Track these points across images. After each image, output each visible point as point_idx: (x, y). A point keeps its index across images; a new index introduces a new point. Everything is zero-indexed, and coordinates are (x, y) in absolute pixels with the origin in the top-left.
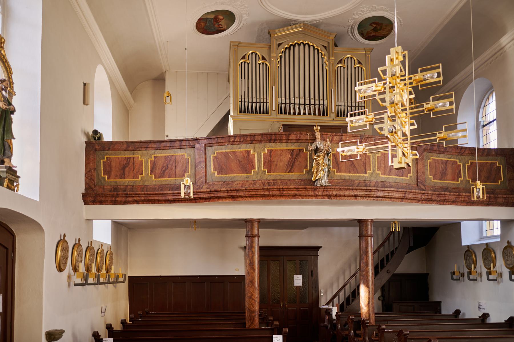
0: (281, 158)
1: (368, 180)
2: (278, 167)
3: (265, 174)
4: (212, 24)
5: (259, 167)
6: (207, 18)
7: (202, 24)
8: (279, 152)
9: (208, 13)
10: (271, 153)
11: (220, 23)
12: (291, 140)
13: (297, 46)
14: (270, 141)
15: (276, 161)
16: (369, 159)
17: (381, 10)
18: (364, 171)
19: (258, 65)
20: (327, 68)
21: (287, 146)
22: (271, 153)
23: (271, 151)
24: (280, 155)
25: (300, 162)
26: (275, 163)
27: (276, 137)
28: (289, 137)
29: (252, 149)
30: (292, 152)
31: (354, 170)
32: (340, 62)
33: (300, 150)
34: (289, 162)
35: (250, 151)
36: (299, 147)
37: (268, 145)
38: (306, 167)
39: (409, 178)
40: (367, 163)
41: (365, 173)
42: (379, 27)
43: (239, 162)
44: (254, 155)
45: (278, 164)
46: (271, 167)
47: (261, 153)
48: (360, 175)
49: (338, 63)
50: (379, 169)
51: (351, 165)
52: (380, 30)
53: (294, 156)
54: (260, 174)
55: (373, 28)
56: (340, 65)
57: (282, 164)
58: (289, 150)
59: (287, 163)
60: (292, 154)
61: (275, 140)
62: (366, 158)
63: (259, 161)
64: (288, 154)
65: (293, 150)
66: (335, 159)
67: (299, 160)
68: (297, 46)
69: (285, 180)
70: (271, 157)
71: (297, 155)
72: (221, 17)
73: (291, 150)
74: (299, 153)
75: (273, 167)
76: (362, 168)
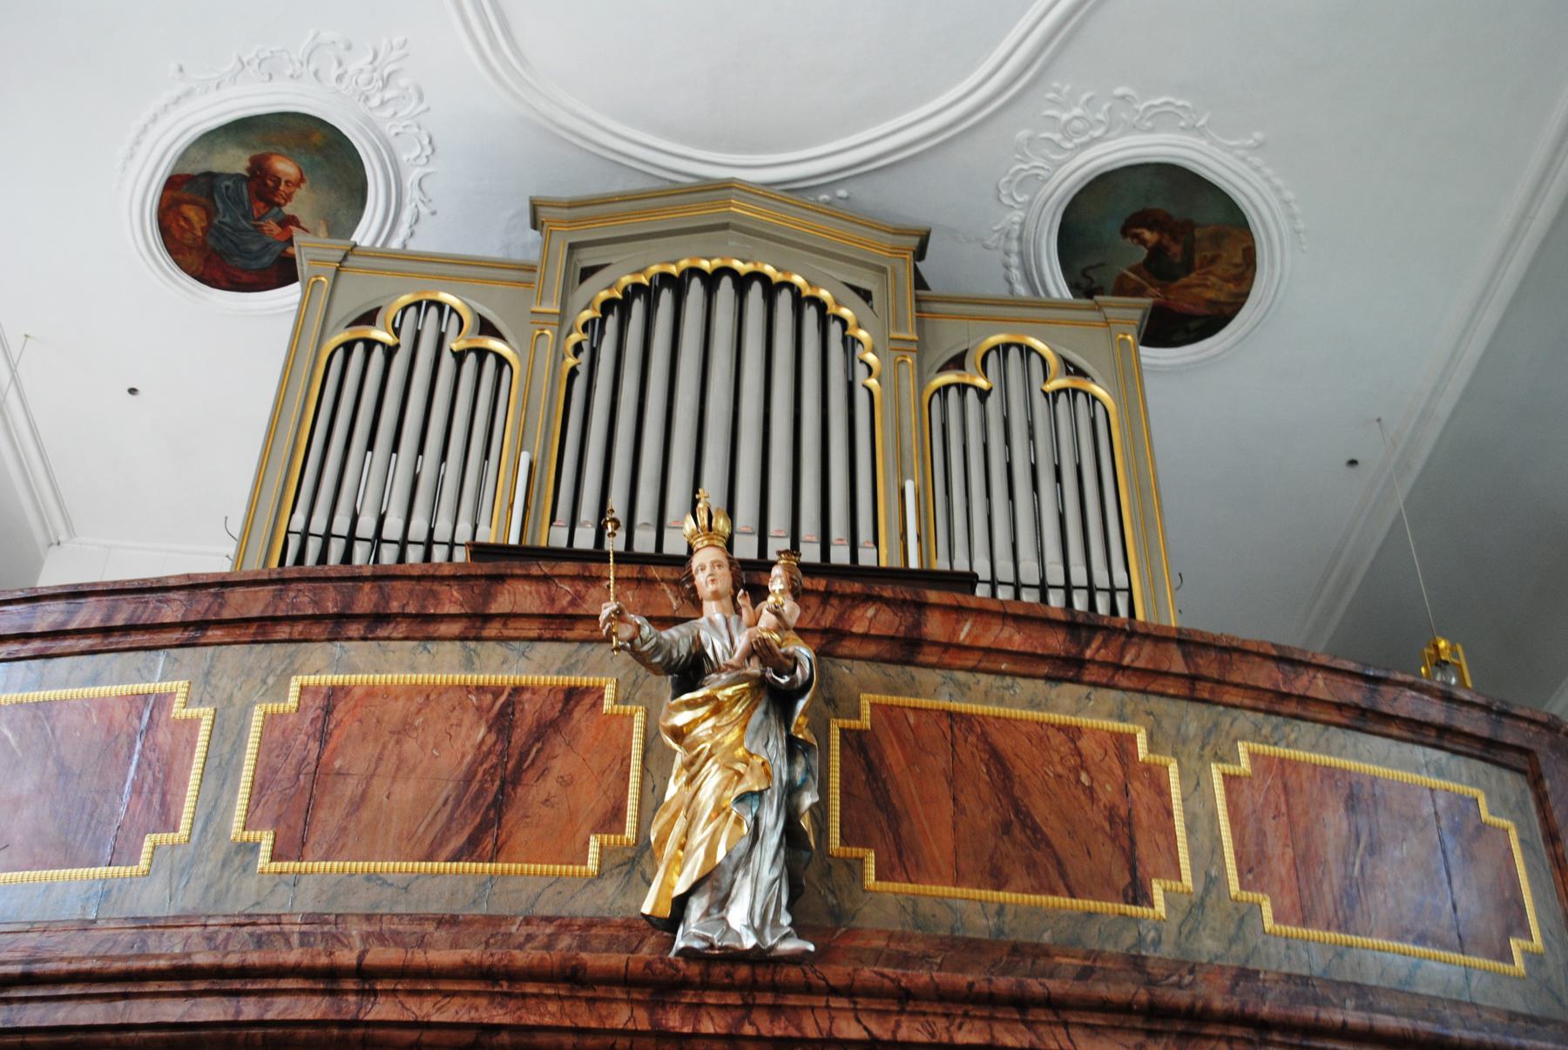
0: (410, 746)
1: (1167, 950)
2: (366, 814)
3: (246, 868)
4: (242, 208)
5: (212, 814)
6: (210, 176)
7: (192, 212)
8: (398, 707)
9: (212, 139)
10: (328, 710)
11: (288, 209)
12: (506, 617)
13: (696, 288)
14: (336, 625)
15: (360, 767)
16: (1163, 792)
17: (1162, 118)
18: (1122, 879)
19: (447, 362)
20: (873, 382)
21: (469, 665)
22: (328, 710)
23: (334, 694)
24: (404, 729)
25: (566, 782)
26: (350, 788)
27: (386, 599)
28: (488, 597)
29: (166, 677)
30: (503, 709)
31: (1031, 866)
32: (958, 362)
33: (572, 695)
34: (468, 778)
35: (162, 701)
36: (568, 669)
37: (318, 653)
38: (613, 819)
39: (1519, 964)
40: (1142, 815)
41: (1139, 894)
42: (1176, 249)
43: (63, 771)
44: (194, 724)
45: (379, 790)
46: (310, 809)
47: (246, 713)
48: (1091, 905)
49: (944, 369)
50: (1251, 869)
51: (1006, 828)
52: (1188, 267)
53: (519, 736)
54: (208, 867)
55: (1143, 253)
56: (950, 377)
57: (406, 792)
58: (480, 689)
59: (448, 789)
60: (503, 722)
61: (377, 620)
62: (1136, 787)
63: (221, 769)
64: (469, 718)
65: (518, 690)
66: (870, 768)
67: (558, 766)
68: (696, 288)
69: (421, 919)
70: (323, 737)
71: (545, 730)
72: (285, 167)
73: (497, 691)
74: (566, 713)
75: (329, 818)
76: (1108, 857)
